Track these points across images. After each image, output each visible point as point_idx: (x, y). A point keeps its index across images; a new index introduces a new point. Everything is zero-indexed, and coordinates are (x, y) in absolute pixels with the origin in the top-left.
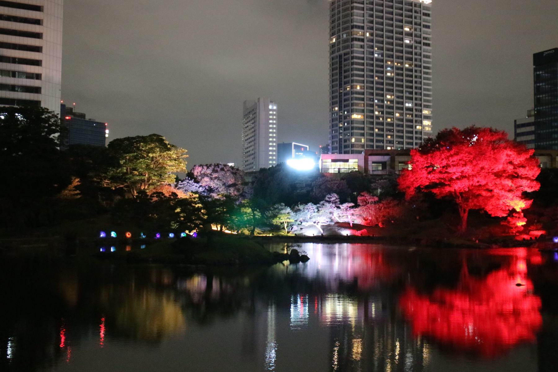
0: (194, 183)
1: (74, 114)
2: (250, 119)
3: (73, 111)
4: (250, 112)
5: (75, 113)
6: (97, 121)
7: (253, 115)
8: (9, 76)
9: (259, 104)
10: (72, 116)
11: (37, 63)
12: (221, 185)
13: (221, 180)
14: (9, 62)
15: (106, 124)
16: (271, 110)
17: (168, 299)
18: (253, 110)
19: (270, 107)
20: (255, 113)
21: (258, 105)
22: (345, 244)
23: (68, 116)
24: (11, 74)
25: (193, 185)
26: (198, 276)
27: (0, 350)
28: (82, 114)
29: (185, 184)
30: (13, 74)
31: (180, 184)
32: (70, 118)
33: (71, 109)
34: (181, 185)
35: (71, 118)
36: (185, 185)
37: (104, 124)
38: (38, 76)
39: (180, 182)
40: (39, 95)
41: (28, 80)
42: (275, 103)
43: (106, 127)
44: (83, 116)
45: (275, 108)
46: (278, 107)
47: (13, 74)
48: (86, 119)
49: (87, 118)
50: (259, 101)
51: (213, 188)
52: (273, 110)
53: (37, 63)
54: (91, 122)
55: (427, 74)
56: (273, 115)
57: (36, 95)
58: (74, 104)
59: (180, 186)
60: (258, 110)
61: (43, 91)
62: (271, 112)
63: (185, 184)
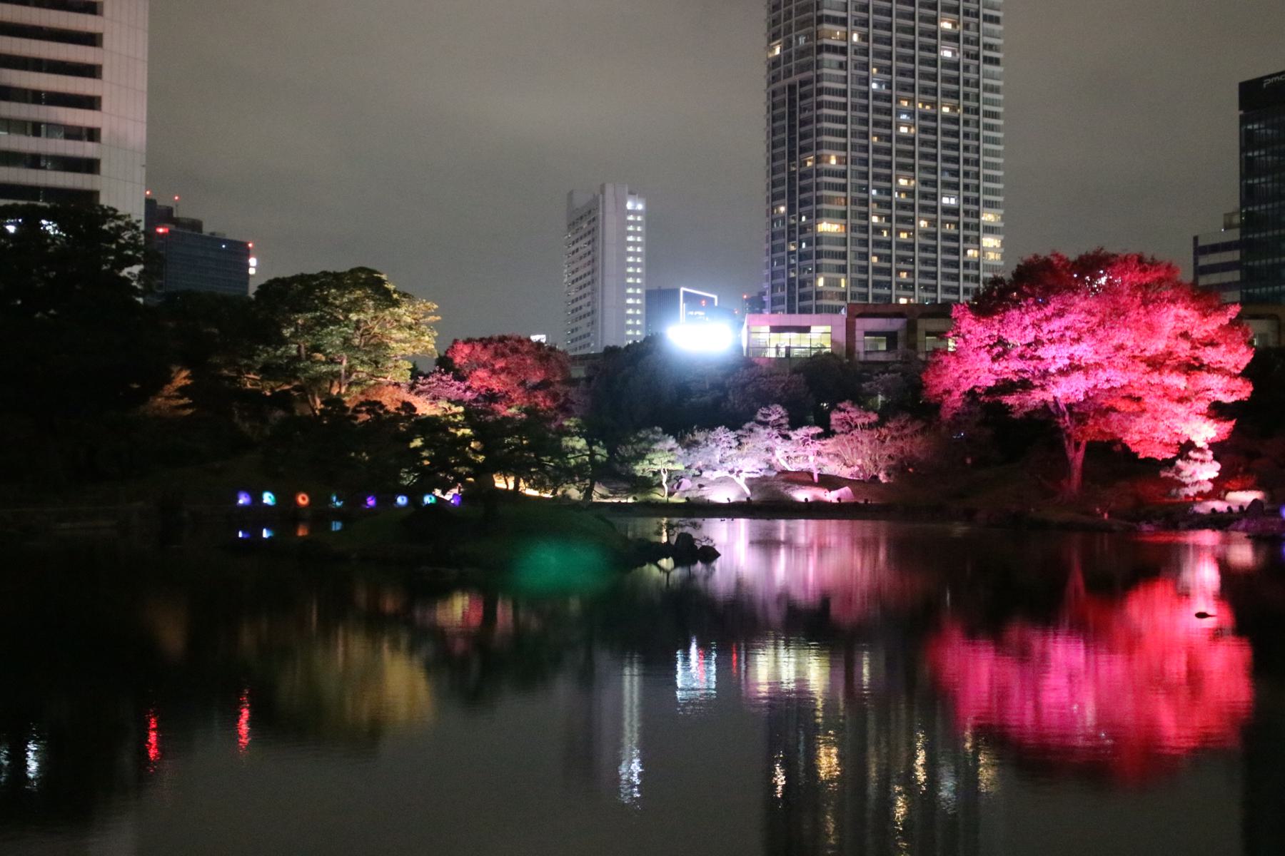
0: (452, 381)
1: (176, 222)
3: (175, 215)
4: (581, 218)
6: (229, 236)
7: (589, 223)
8: (26, 134)
10: (173, 227)
11: (91, 103)
13: (514, 374)
14: (25, 101)
15: (250, 245)
17: (395, 646)
18: (590, 212)
19: (629, 205)
20: (594, 219)
21: (601, 201)
23: (163, 227)
25: (451, 386)
30: (36, 129)
33: (170, 210)
34: (423, 384)
36: (432, 385)
37: (246, 244)
38: (92, 134)
39: (421, 378)
40: (95, 177)
41: (71, 143)
42: (639, 197)
43: (251, 252)
44: (196, 225)
45: (640, 207)
46: (647, 206)
47: (36, 129)
50: (603, 192)
52: (635, 213)
53: (91, 103)
54: (215, 240)
57: (87, 177)
59: (421, 388)
60: (601, 213)
62: (631, 218)
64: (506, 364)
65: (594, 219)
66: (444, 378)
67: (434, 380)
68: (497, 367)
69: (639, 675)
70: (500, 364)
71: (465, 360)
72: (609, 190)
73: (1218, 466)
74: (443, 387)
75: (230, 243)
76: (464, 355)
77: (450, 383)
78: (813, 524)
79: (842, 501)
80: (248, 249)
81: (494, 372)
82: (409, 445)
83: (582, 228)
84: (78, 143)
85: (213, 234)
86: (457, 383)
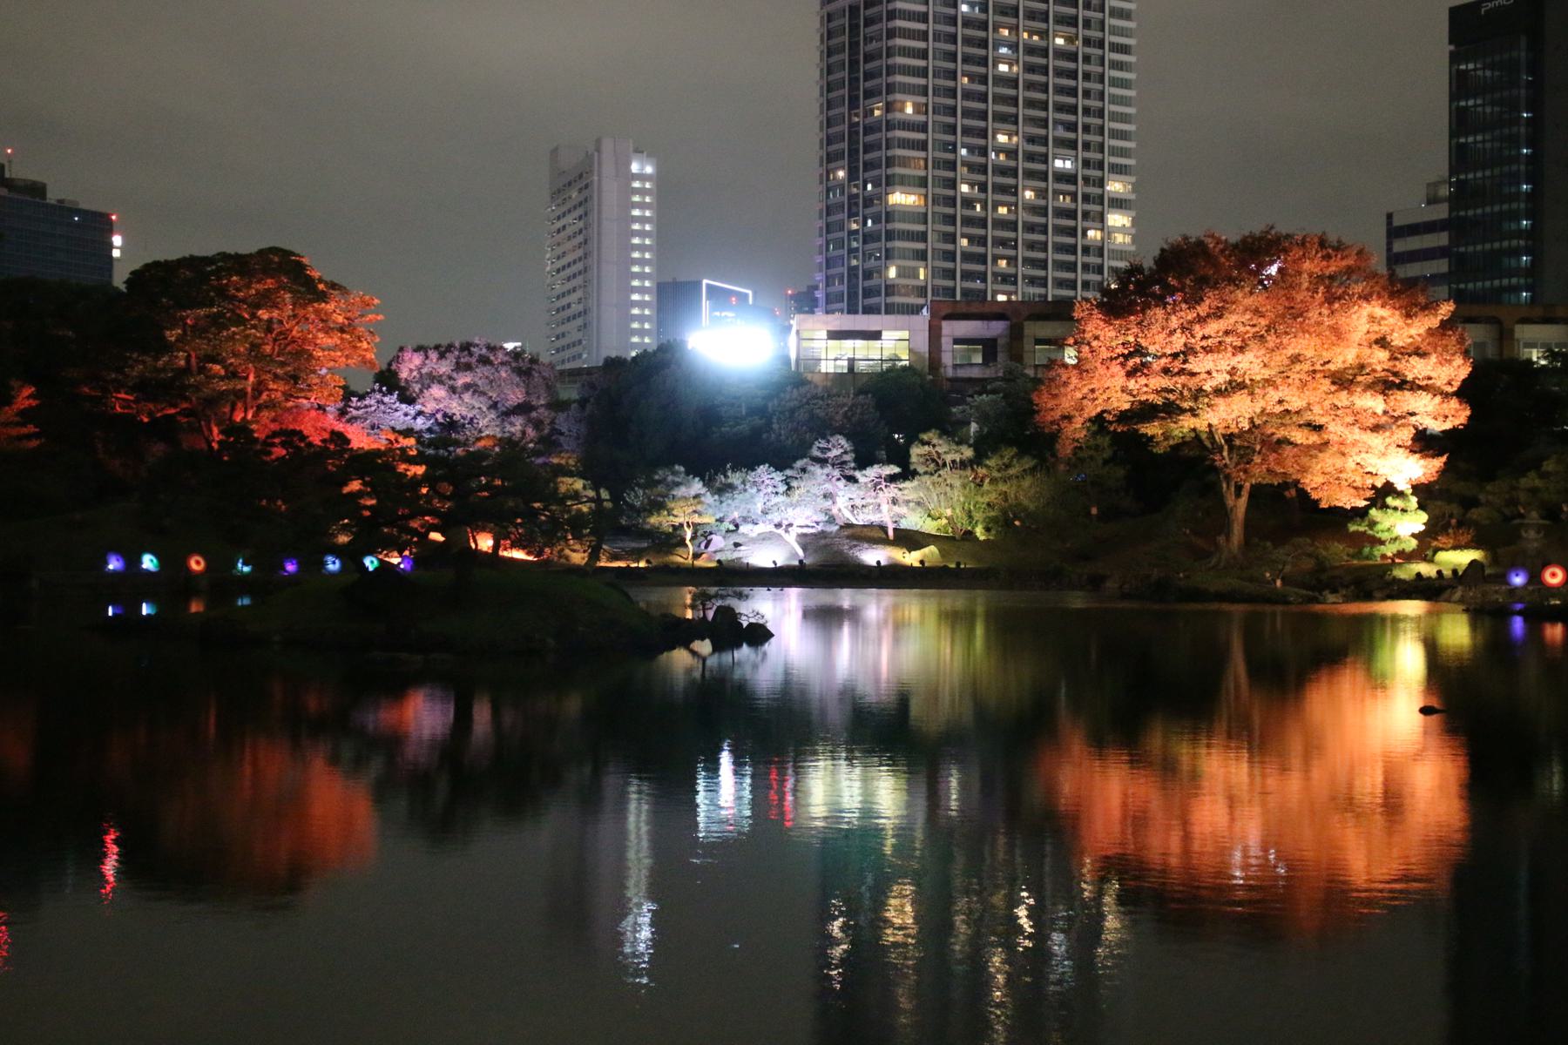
0: (398, 404)
2: (569, 205)
4: (570, 184)
5: (12, 180)
6: (84, 206)
7: (580, 190)
13: (483, 394)
18: (581, 176)
19: (635, 167)
20: (587, 186)
25: (396, 410)
28: (34, 183)
31: (354, 405)
34: (357, 409)
36: (369, 410)
39: (354, 399)
43: (115, 228)
44: (38, 190)
45: (649, 170)
48: (48, 201)
49: (52, 196)
50: (598, 150)
52: (642, 177)
54: (64, 210)
55: (1122, 70)
59: (355, 413)
65: (587, 186)
72: (607, 146)
74: (384, 412)
77: (394, 407)
79: (926, 565)
81: (453, 390)
83: (570, 198)
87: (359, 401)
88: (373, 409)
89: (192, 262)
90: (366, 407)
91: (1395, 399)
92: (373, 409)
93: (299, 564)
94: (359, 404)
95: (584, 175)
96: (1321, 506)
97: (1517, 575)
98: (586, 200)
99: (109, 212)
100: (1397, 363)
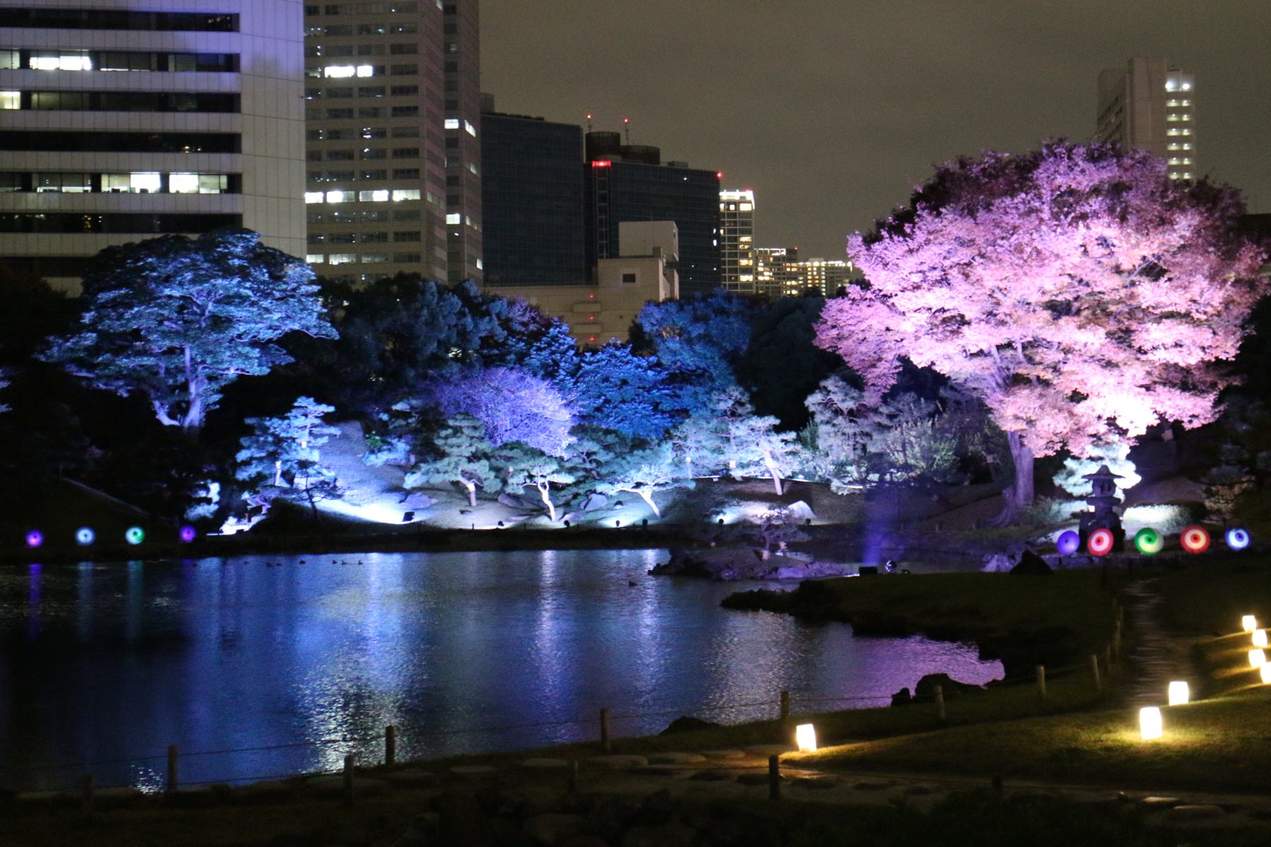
0: (630, 357)
1: (626, 152)
3: (623, 142)
4: (1109, 108)
5: (628, 147)
6: (693, 166)
9: (1132, 80)
10: (618, 159)
12: (717, 359)
14: (148, 27)
16: (1171, 96)
18: (1117, 99)
19: (1170, 86)
20: (1121, 110)
21: (1128, 80)
22: (251, 559)
24: (154, 60)
25: (627, 363)
26: (663, 629)
27: (1179, 846)
28: (648, 148)
29: (603, 360)
30: (161, 61)
31: (587, 360)
32: (610, 164)
34: (590, 363)
35: (612, 163)
36: (600, 364)
38: (230, 63)
39: (588, 354)
41: (203, 75)
42: (1184, 73)
43: (721, 182)
44: (652, 155)
45: (1186, 87)
47: (161, 61)
48: (662, 165)
49: (665, 159)
50: (1131, 72)
51: (694, 368)
52: (1178, 95)
54: (675, 171)
55: (163, 67)
56: (1179, 111)
57: (225, 116)
58: (589, 117)
59: (587, 367)
60: (1128, 101)
61: (245, 103)
63: (603, 360)
64: (705, 330)
65: (1121, 110)
66: (618, 353)
67: (604, 357)
68: (694, 335)
69: (937, 694)
70: (698, 330)
71: (655, 328)
73: (1065, 463)
75: (694, 174)
76: (653, 321)
77: (625, 360)
78: (489, 556)
79: (572, 524)
80: (717, 180)
82: (780, 424)
83: (1110, 123)
84: (213, 75)
85: (671, 164)
86: (635, 359)
87: (592, 356)
88: (604, 363)
89: (308, 223)
90: (598, 362)
91: (667, 310)
92: (604, 363)
93: (25, 542)
94: (592, 359)
95: (1119, 98)
96: (1054, 478)
97: (188, 533)
98: (1121, 125)
99: (713, 169)
100: (919, 261)
